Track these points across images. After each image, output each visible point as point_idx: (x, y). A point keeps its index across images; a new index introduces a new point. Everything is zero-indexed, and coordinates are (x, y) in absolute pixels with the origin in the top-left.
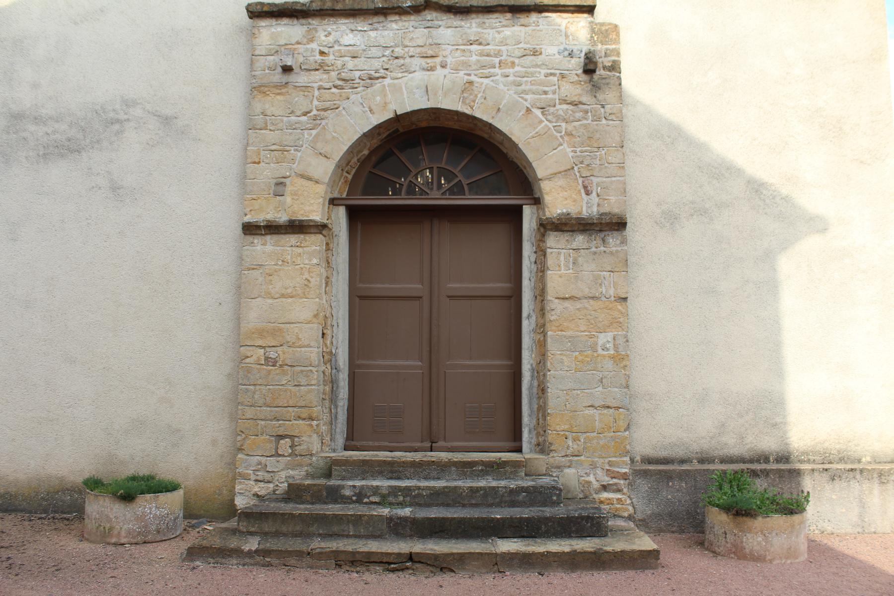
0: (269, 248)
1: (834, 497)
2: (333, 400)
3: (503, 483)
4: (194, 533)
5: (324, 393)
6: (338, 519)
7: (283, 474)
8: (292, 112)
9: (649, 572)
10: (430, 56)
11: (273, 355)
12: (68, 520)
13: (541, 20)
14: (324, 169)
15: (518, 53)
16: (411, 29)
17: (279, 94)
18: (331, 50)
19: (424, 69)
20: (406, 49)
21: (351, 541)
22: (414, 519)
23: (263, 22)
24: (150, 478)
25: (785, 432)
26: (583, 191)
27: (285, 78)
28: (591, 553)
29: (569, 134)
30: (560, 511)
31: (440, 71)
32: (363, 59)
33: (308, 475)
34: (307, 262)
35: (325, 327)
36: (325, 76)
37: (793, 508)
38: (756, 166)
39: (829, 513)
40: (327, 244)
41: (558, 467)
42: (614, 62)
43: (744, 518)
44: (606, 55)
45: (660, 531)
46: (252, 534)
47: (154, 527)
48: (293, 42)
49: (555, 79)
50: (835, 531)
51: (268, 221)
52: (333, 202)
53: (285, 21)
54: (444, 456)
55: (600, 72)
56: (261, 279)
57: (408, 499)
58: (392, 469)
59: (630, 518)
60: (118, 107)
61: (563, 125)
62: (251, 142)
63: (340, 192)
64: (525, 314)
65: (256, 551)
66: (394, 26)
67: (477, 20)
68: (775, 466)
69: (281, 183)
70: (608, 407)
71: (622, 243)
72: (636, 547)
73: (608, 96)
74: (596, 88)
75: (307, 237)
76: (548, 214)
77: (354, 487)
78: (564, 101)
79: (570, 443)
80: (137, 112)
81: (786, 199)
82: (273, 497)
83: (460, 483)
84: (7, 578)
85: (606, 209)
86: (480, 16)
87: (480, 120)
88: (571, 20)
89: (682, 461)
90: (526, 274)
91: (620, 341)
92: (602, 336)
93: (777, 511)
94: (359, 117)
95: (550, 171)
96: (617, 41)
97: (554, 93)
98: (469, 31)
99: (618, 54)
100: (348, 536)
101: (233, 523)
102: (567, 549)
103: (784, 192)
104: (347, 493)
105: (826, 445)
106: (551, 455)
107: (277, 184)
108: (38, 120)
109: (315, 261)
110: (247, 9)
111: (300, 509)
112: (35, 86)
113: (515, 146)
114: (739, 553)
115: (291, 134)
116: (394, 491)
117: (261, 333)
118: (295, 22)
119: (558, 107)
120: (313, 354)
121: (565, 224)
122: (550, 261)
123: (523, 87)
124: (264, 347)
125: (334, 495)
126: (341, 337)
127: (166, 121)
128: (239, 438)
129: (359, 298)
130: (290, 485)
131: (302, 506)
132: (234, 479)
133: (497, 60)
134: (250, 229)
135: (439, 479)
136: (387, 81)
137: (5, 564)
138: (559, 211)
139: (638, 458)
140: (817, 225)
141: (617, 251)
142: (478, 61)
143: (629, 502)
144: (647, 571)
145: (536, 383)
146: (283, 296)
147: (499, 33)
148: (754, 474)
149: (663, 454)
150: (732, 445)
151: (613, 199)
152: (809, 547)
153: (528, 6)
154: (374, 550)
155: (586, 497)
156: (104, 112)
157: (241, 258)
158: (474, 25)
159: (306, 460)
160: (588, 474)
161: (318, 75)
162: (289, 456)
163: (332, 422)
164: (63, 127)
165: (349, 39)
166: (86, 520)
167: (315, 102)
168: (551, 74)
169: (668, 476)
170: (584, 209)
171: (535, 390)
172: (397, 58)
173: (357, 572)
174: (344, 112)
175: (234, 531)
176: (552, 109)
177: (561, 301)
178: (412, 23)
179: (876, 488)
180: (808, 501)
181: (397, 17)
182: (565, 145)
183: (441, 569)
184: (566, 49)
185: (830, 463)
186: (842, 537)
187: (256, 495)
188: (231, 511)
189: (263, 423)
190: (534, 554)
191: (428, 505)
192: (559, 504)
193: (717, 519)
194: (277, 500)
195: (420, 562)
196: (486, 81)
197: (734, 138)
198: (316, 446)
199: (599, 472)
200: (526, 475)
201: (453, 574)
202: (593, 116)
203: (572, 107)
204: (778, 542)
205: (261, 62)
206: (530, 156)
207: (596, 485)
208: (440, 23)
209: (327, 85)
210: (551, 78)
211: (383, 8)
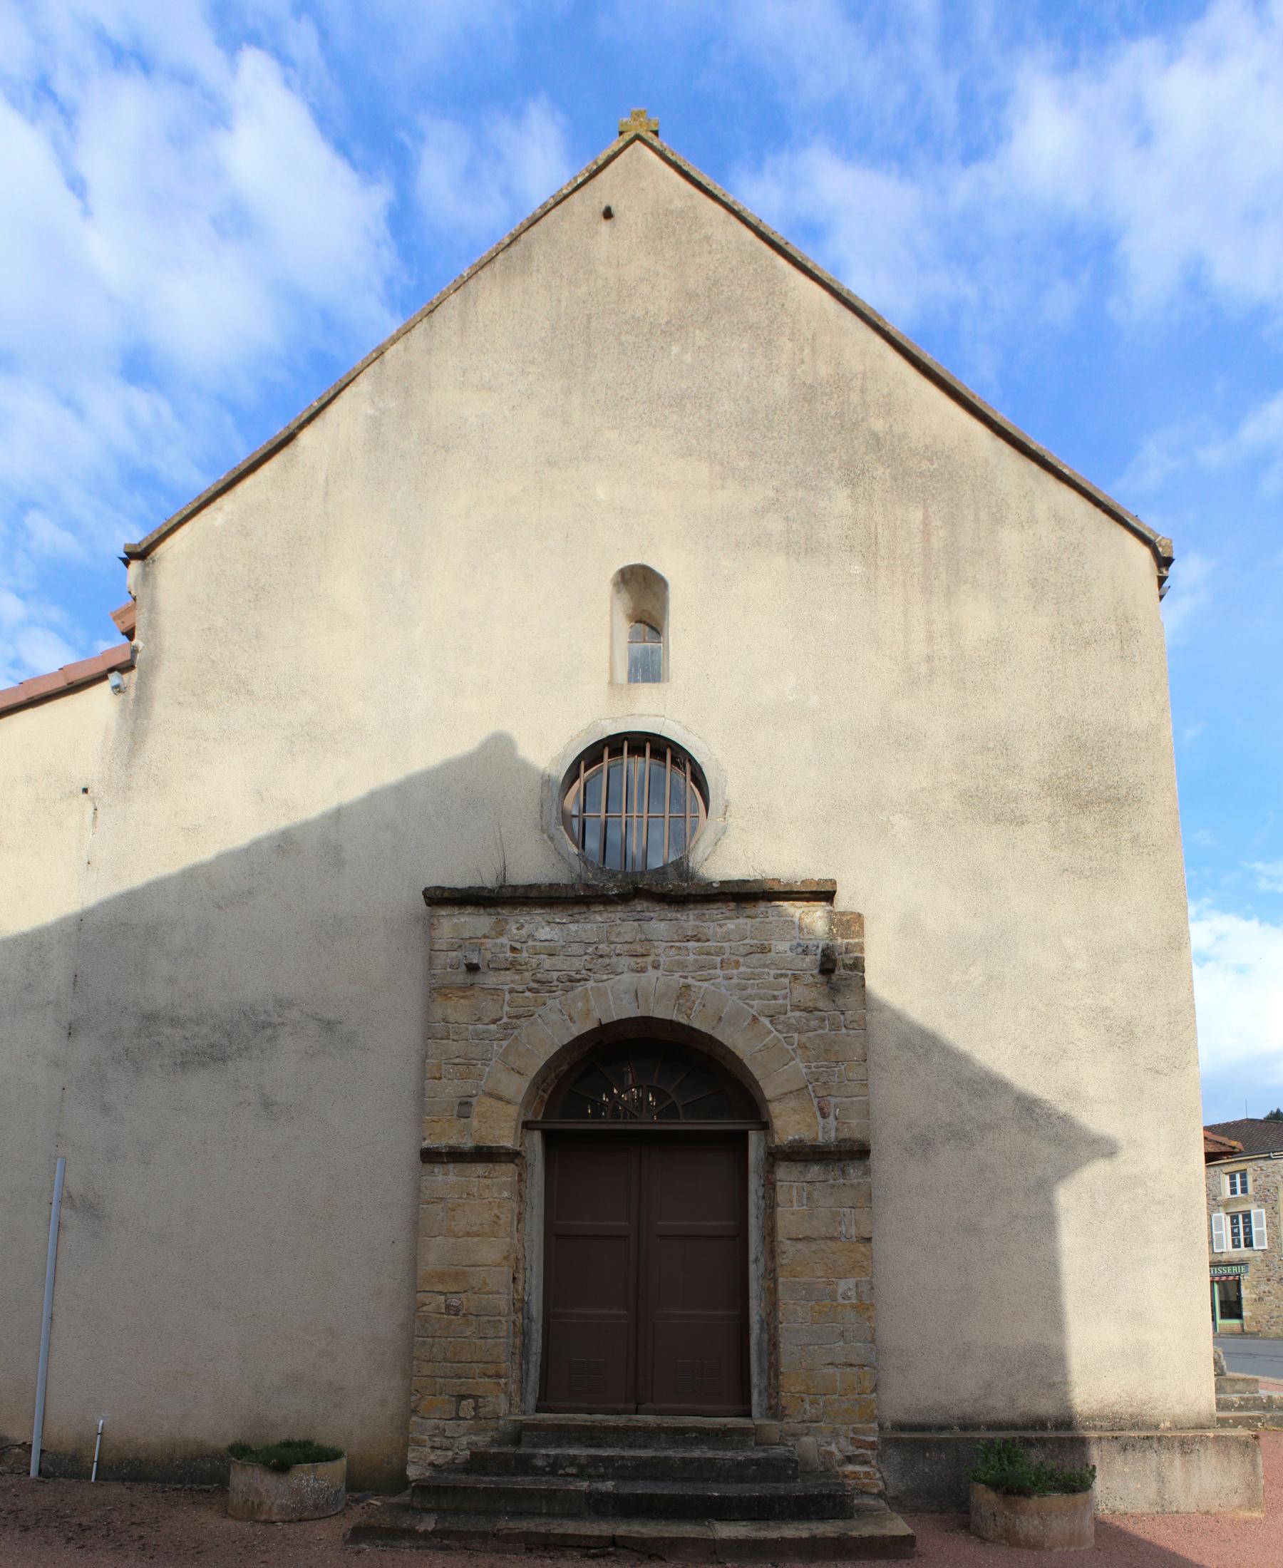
0: (452, 1178)
1: (1127, 1470)
2: (525, 1353)
3: (729, 1454)
4: (357, 1509)
5: (514, 1347)
6: (529, 1494)
7: (464, 1440)
8: (479, 1019)
9: (903, 1562)
10: (641, 954)
11: (455, 1302)
12: (208, 1491)
13: (770, 911)
14: (517, 1087)
15: (743, 951)
16: (618, 922)
17: (462, 997)
18: (524, 945)
19: (633, 970)
20: (612, 946)
21: (544, 1520)
22: (617, 1495)
23: (443, 912)
24: (306, 1444)
25: (1066, 1393)
26: (818, 1114)
27: (470, 979)
28: (833, 1538)
29: (802, 1046)
30: (797, 1488)
32: (562, 957)
33: (494, 1442)
34: (496, 1195)
35: (516, 1271)
36: (517, 977)
37: (1077, 1483)
38: (1026, 1076)
39: (1121, 1489)
40: (520, 1175)
41: (794, 1435)
42: (857, 958)
43: (1017, 1498)
44: (847, 951)
45: (916, 1511)
46: (428, 1511)
47: (311, 1502)
48: (480, 935)
49: (787, 981)
50: (1130, 1511)
51: (451, 1147)
52: (527, 1126)
53: (470, 910)
54: (651, 1420)
55: (840, 971)
56: (442, 1214)
57: (610, 1470)
58: (591, 1436)
59: (880, 1495)
60: (270, 1008)
61: (796, 1035)
62: (430, 1053)
63: (535, 1114)
64: (752, 1257)
65: (434, 1532)
66: (599, 918)
67: (696, 912)
68: (1053, 1434)
69: (467, 1103)
70: (851, 1365)
71: (865, 1174)
72: (887, 1532)
73: (850, 1000)
74: (834, 991)
75: (497, 1167)
76: (777, 1142)
77: (548, 1456)
78: (796, 1007)
79: (807, 1407)
80: (293, 1014)
81: (1065, 1119)
82: (452, 1467)
83: (670, 1453)
84: (141, 1560)
85: (846, 1134)
86: (699, 906)
87: (699, 1032)
88: (806, 910)
89: (941, 1428)
90: (752, 1210)
91: (864, 1288)
92: (842, 1282)
93: (1055, 1489)
94: (556, 1028)
95: (780, 1091)
96: (861, 933)
97: (785, 997)
98: (685, 924)
99: (862, 950)
100: (540, 1515)
101: (404, 1498)
102: (805, 1534)
103: (1062, 1109)
104: (540, 1463)
105: (1116, 1408)
106: (786, 1420)
107: (461, 1104)
108: (174, 1022)
109: (506, 1194)
110: (425, 897)
111: (485, 1482)
112: (172, 981)
113: (739, 1061)
114: (1012, 1539)
115: (477, 1045)
116: (594, 1460)
117: (441, 1277)
118: (482, 911)
119: (790, 1014)
120: (502, 1302)
121: (798, 1153)
122: (781, 1196)
123: (749, 991)
124: (445, 1294)
125: (524, 1465)
126: (534, 1283)
127: (329, 1026)
128: (413, 1398)
129: (555, 1237)
130: (472, 1454)
131: (486, 1478)
132: (406, 1446)
133: (719, 959)
134: (429, 1156)
135: (645, 1447)
136: (590, 984)
137: (138, 1544)
138: (790, 1138)
139: (888, 1424)
140: (1105, 1148)
141: (859, 1184)
142: (696, 960)
143: (878, 1475)
144: (900, 1561)
145: (766, 1337)
146: (468, 1234)
147: (721, 926)
148: (1029, 1443)
149: (918, 1419)
150: (1000, 1408)
151: (854, 1122)
152: (1096, 1531)
153: (755, 894)
154: (570, 1531)
155: (827, 1470)
156: (254, 1014)
157: (418, 1189)
158: (691, 917)
159: (492, 1424)
160: (829, 1444)
161: (508, 976)
162: (473, 1418)
163: (522, 1380)
164: (205, 1030)
165: (545, 933)
166: (231, 1494)
167: (506, 1008)
168: (782, 975)
169: (924, 1446)
170: (820, 1135)
171: (765, 1345)
172: (601, 956)
173: (551, 1558)
174: (539, 1020)
175: (407, 1508)
176: (782, 1018)
177: (793, 1243)
178: (619, 915)
179: (1178, 1460)
180: (1094, 1477)
181: (601, 908)
182: (798, 1059)
183: (650, 1557)
184: (799, 945)
185: (1122, 1429)
186: (1137, 1518)
187: (432, 1464)
188: (399, 1482)
189: (442, 1380)
190: (766, 1540)
191: (633, 1478)
192: (795, 1478)
193: (985, 1498)
194: (456, 1471)
195: (624, 1547)
196: (705, 985)
197: (1002, 1047)
198: (503, 1408)
199: (842, 1440)
200: (756, 1444)
201: (663, 1563)
202: (831, 1024)
203: (806, 1014)
204: (1059, 1526)
205: (442, 959)
206: (757, 1073)
207: (838, 1456)
208: (652, 915)
209: (520, 988)
210: (782, 980)
211: (584, 896)
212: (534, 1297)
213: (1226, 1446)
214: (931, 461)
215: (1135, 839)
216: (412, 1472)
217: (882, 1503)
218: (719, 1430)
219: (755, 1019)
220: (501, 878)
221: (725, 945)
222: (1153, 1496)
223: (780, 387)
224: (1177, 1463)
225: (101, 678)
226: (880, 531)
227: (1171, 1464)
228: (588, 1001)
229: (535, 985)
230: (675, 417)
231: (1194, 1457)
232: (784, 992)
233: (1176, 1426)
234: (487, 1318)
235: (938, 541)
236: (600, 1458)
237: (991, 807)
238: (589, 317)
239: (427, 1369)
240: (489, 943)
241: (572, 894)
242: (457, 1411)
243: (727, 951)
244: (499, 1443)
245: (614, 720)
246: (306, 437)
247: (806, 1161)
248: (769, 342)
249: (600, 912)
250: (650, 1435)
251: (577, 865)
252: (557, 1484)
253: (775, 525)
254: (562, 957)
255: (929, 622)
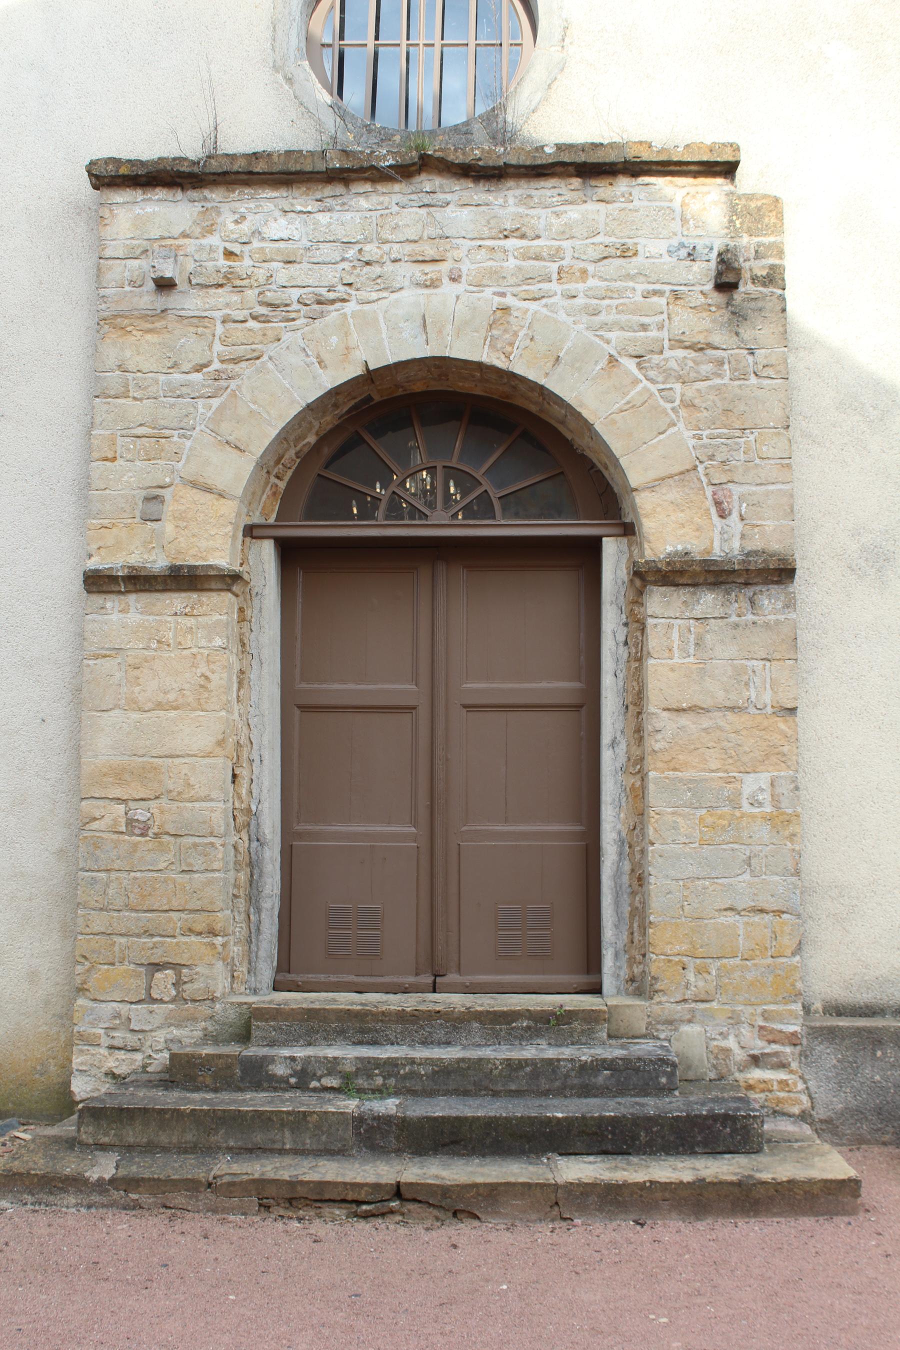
2: (253, 897)
3: (567, 1052)
6: (263, 1119)
7: (161, 1036)
8: (175, 365)
11: (141, 815)
13: (636, 191)
14: (235, 471)
16: (395, 209)
18: (246, 248)
20: (386, 247)
21: (288, 1160)
22: (404, 1119)
26: (713, 510)
27: (162, 301)
28: (732, 1183)
29: (689, 405)
30: (674, 1105)
32: (305, 266)
33: (208, 1037)
34: (203, 643)
35: (237, 763)
36: (235, 298)
40: (241, 610)
41: (670, 1022)
42: (772, 267)
44: (758, 256)
46: (103, 1147)
48: (176, 232)
49: (663, 301)
51: (133, 568)
53: (160, 193)
54: (457, 1001)
55: (746, 287)
56: (118, 675)
57: (392, 1081)
58: (362, 1027)
59: (804, 1117)
61: (678, 387)
62: (98, 420)
64: (606, 738)
65: (112, 1181)
66: (363, 203)
67: (518, 192)
69: (156, 498)
70: (762, 911)
72: (816, 1174)
73: (761, 332)
75: (205, 597)
76: (649, 555)
77: (293, 1059)
78: (678, 343)
79: (691, 977)
83: (487, 1052)
85: (756, 544)
86: (523, 182)
88: (692, 190)
90: (608, 664)
91: (784, 788)
92: (749, 779)
94: (300, 374)
95: (652, 475)
96: (778, 228)
97: (661, 327)
99: (781, 253)
100: (282, 1152)
101: (68, 1128)
102: (687, 1177)
104: (280, 1070)
106: (657, 999)
107: (147, 499)
109: (218, 642)
110: (90, 174)
111: (194, 1102)
113: (588, 426)
115: (172, 406)
116: (367, 1067)
117: (119, 774)
118: (179, 194)
119: (667, 353)
121: (682, 572)
123: (602, 317)
124: (125, 801)
125: (255, 1075)
126: (266, 784)
128: (79, 969)
129: (303, 712)
130: (173, 1057)
131: (196, 1096)
134: (97, 582)
135: (448, 1043)
136: (350, 307)
138: (669, 549)
139: (818, 1005)
143: (801, 1086)
144: (837, 1219)
145: (627, 866)
146: (159, 706)
147: (557, 215)
149: (864, 997)
151: (769, 525)
154: (329, 1177)
155: (721, 1078)
157: (81, 636)
158: (511, 201)
159: (204, 1009)
161: (222, 296)
162: (173, 1001)
165: (279, 227)
167: (218, 347)
168: (655, 293)
169: (873, 1040)
170: (716, 544)
171: (625, 879)
172: (368, 263)
173: (300, 1220)
174: (270, 365)
175: (71, 1143)
176: (656, 359)
178: (396, 198)
181: (368, 187)
182: (681, 425)
183: (455, 1214)
184: (682, 245)
188: (63, 1103)
189: (123, 940)
190: (625, 1185)
191: (430, 1094)
192: (671, 1090)
194: (150, 1084)
195: (415, 1200)
196: (533, 306)
198: (221, 984)
199: (745, 1030)
200: (610, 1036)
201: (476, 1223)
202: (733, 370)
203: (693, 354)
205: (117, 272)
206: (616, 446)
207: (740, 1055)
208: (448, 197)
210: (655, 299)
211: (342, 170)
212: (265, 806)
216: (81, 1088)
217: (807, 1130)
218: (553, 1013)
220: (210, 143)
221: (566, 244)
228: (347, 334)
229: (263, 310)
232: (659, 318)
234: (191, 840)
236: (376, 1063)
239: (99, 922)
240: (190, 245)
241: (321, 166)
242: (149, 988)
243: (569, 254)
244: (216, 1040)
247: (694, 585)
250: (455, 1024)
251: (330, 121)
252: (305, 1102)
254: (305, 266)
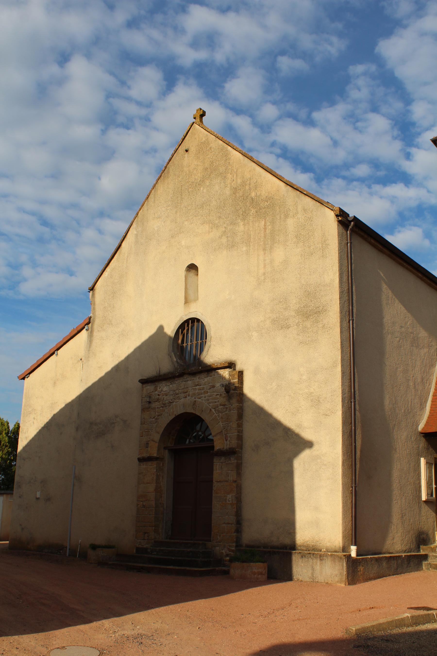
0: (144, 466)
1: (302, 565)
11: (144, 504)
14: (157, 437)
15: (208, 388)
31: (188, 398)
36: (159, 404)
50: (303, 580)
53: (150, 384)
55: (232, 391)
61: (220, 414)
78: (221, 405)
92: (228, 496)
105: (308, 543)
119: (219, 407)
123: (210, 401)
136: (174, 403)
140: (309, 444)
146: (147, 483)
160: (223, 550)
161: (157, 403)
165: (165, 389)
172: (177, 394)
176: (217, 408)
196: (199, 400)
209: (159, 407)
213: (334, 558)
214: (267, 202)
215: (324, 326)
219: (211, 410)
222: (310, 575)
223: (228, 191)
224: (318, 564)
225: (84, 328)
226: (251, 233)
227: (316, 564)
229: (162, 405)
230: (201, 211)
231: (324, 561)
233: (327, 551)
235: (268, 231)
237: (280, 324)
238: (182, 186)
245: (186, 315)
246: (123, 244)
248: (225, 177)
249: (177, 380)
253: (224, 240)
255: (265, 260)
